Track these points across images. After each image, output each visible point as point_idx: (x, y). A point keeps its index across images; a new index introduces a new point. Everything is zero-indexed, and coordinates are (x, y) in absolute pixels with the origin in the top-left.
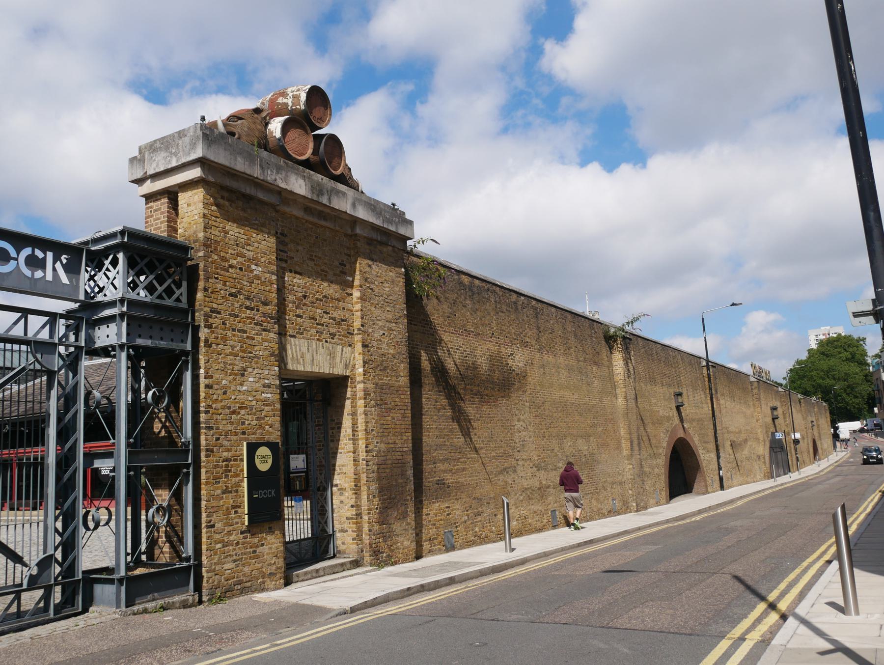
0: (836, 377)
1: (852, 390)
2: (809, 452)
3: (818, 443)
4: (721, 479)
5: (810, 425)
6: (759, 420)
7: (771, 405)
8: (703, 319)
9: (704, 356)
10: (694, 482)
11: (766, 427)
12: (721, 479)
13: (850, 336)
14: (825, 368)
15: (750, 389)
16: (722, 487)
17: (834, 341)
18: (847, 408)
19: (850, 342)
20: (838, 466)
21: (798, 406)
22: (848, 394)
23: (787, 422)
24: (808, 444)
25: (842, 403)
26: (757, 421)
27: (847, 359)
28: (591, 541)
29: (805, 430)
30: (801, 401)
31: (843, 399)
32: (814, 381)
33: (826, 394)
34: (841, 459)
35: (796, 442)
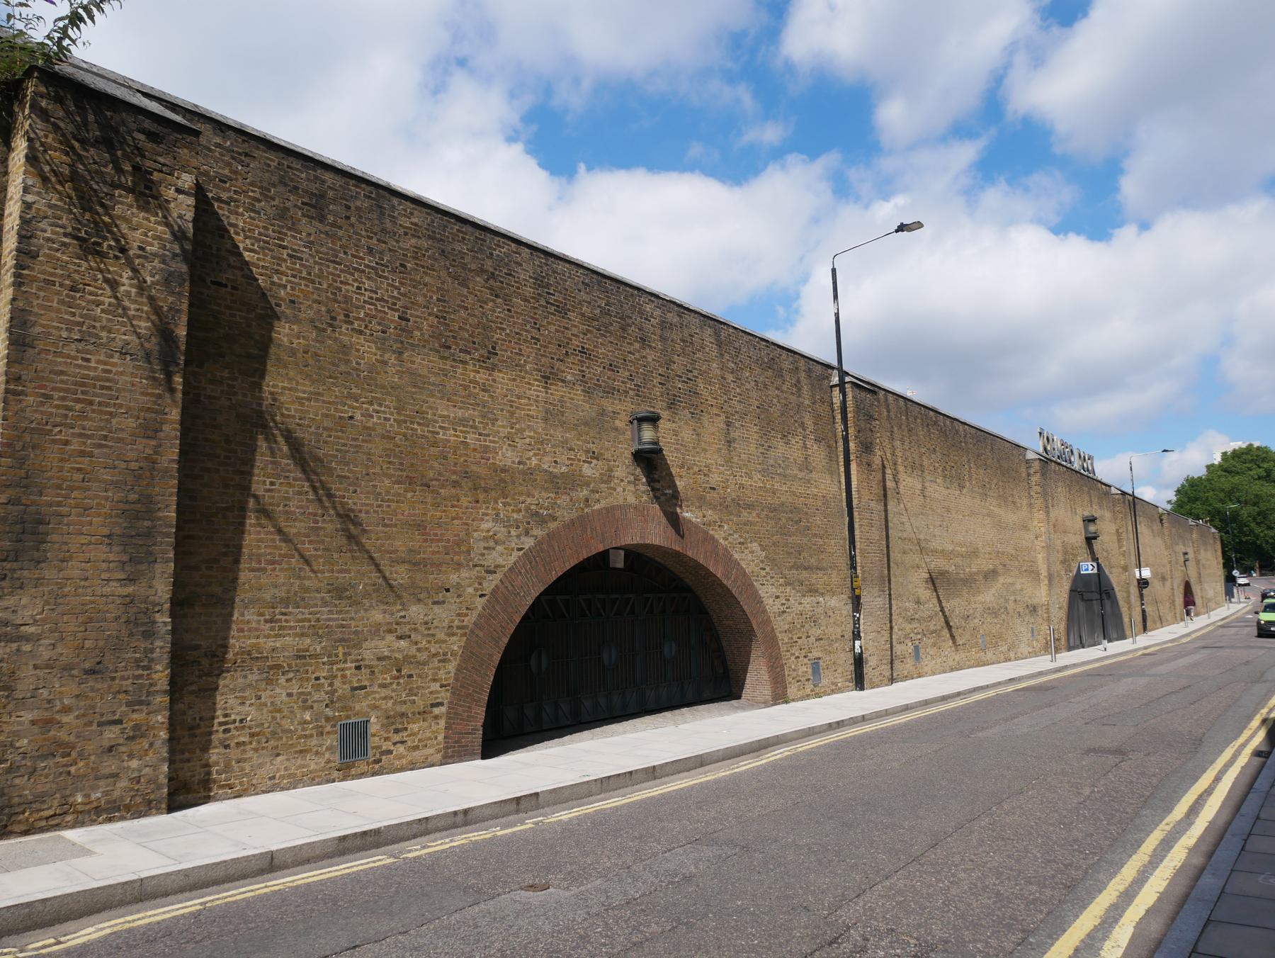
0: (1242, 499)
1: (1264, 518)
2: (1173, 603)
3: (1196, 589)
4: (859, 661)
5: (1182, 559)
6: (1041, 536)
7: (1086, 513)
8: (834, 271)
9: (835, 363)
10: (745, 671)
11: (1066, 553)
12: (859, 661)
13: (1266, 447)
14: (1227, 486)
15: (1024, 475)
16: (859, 682)
17: (1243, 454)
18: (1256, 543)
19: (1264, 455)
20: (1222, 626)
21: (1157, 526)
22: (1258, 524)
23: (1124, 549)
24: (1173, 589)
25: (1248, 535)
26: (1037, 538)
27: (1260, 478)
28: (838, 723)
29: (1168, 566)
30: (1163, 517)
31: (1251, 531)
32: (1210, 505)
33: (1225, 522)
34: (1233, 614)
35: (1143, 583)
